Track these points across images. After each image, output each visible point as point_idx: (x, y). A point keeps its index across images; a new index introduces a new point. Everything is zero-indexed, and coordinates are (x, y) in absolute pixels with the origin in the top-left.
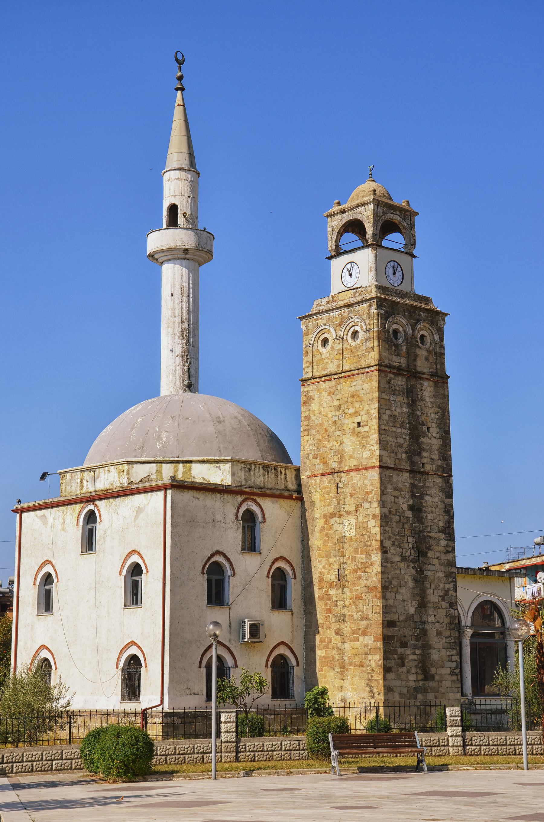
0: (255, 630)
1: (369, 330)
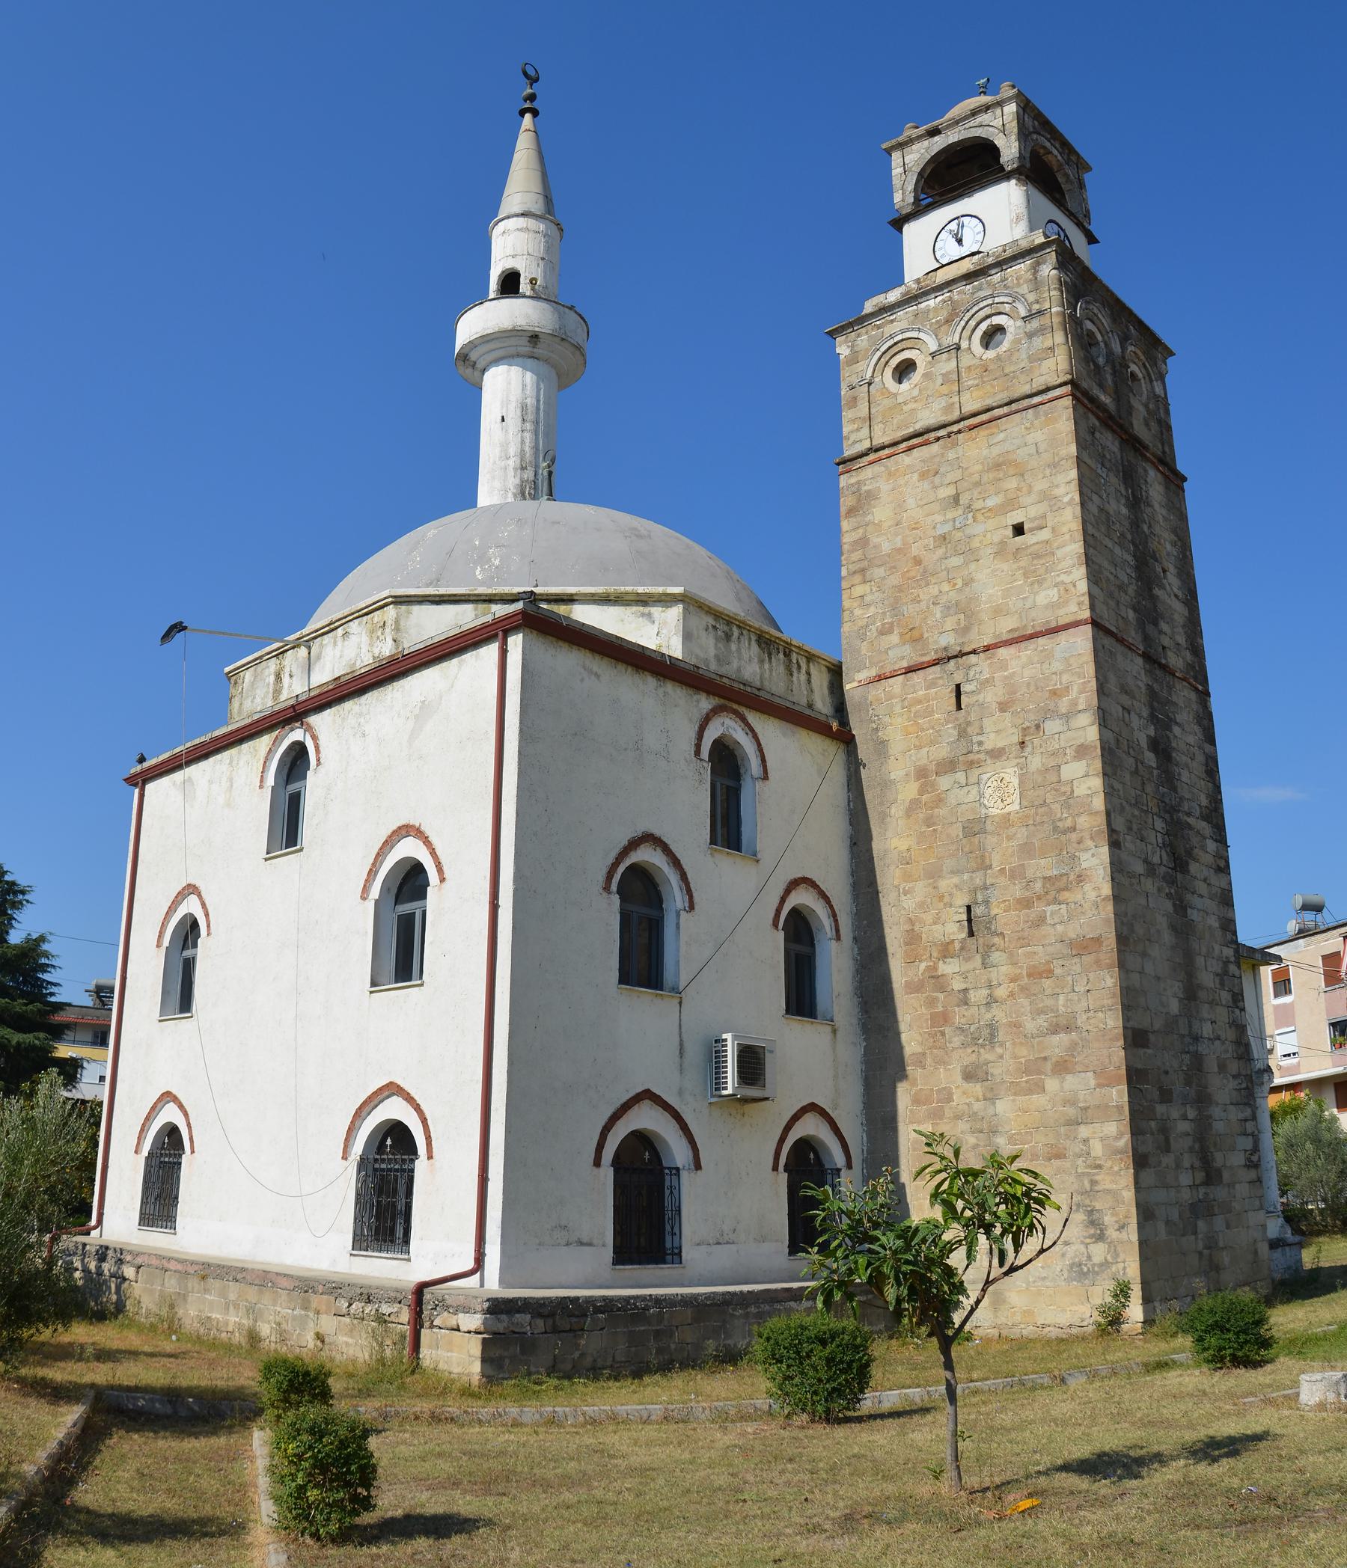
0: (752, 1063)
1: (1040, 312)
